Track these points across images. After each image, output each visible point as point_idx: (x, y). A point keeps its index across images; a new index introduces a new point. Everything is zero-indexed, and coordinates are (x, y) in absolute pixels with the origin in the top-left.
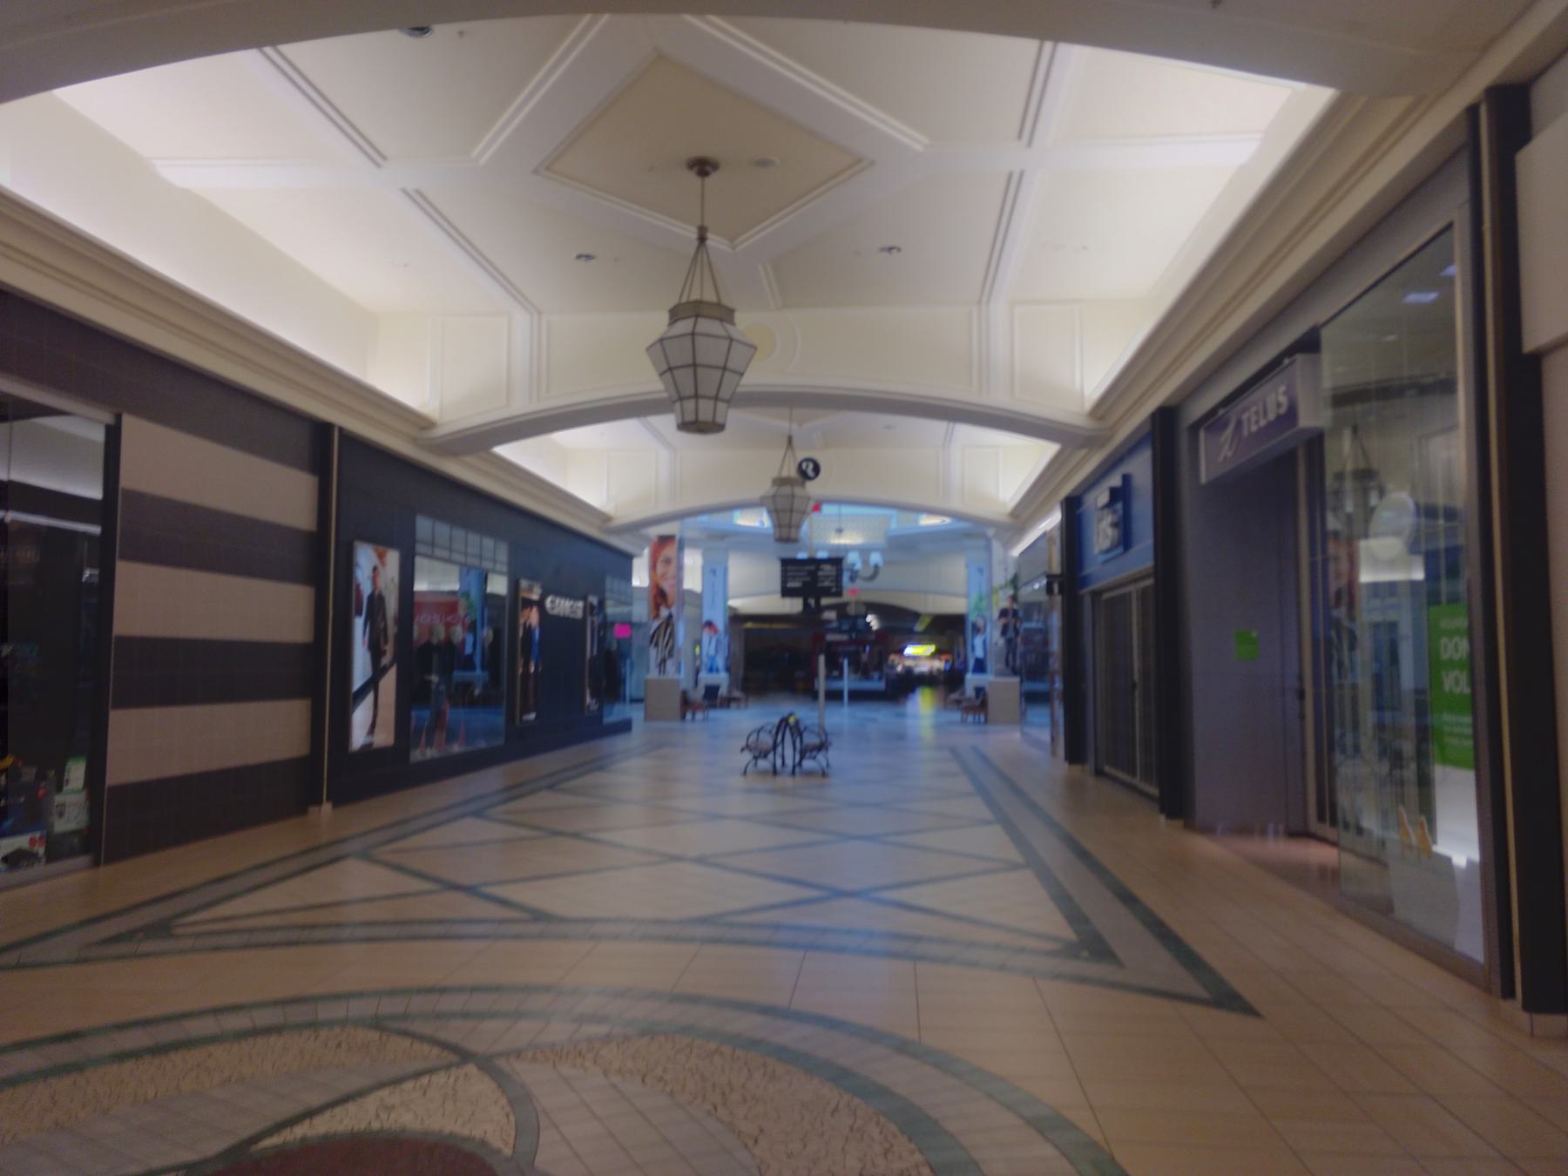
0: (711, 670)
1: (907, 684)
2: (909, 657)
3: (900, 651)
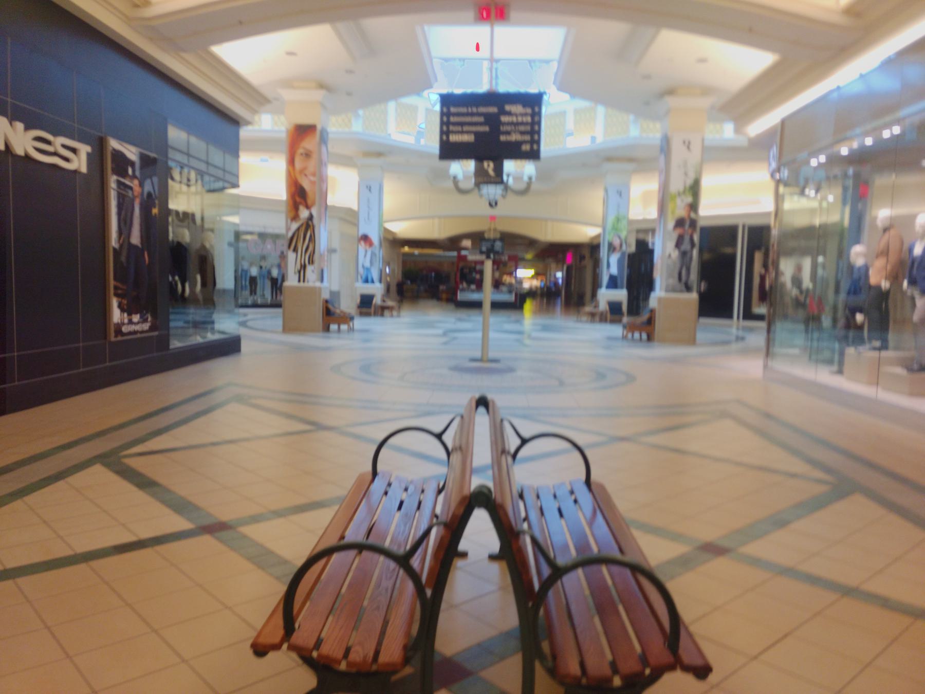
0: (366, 281)
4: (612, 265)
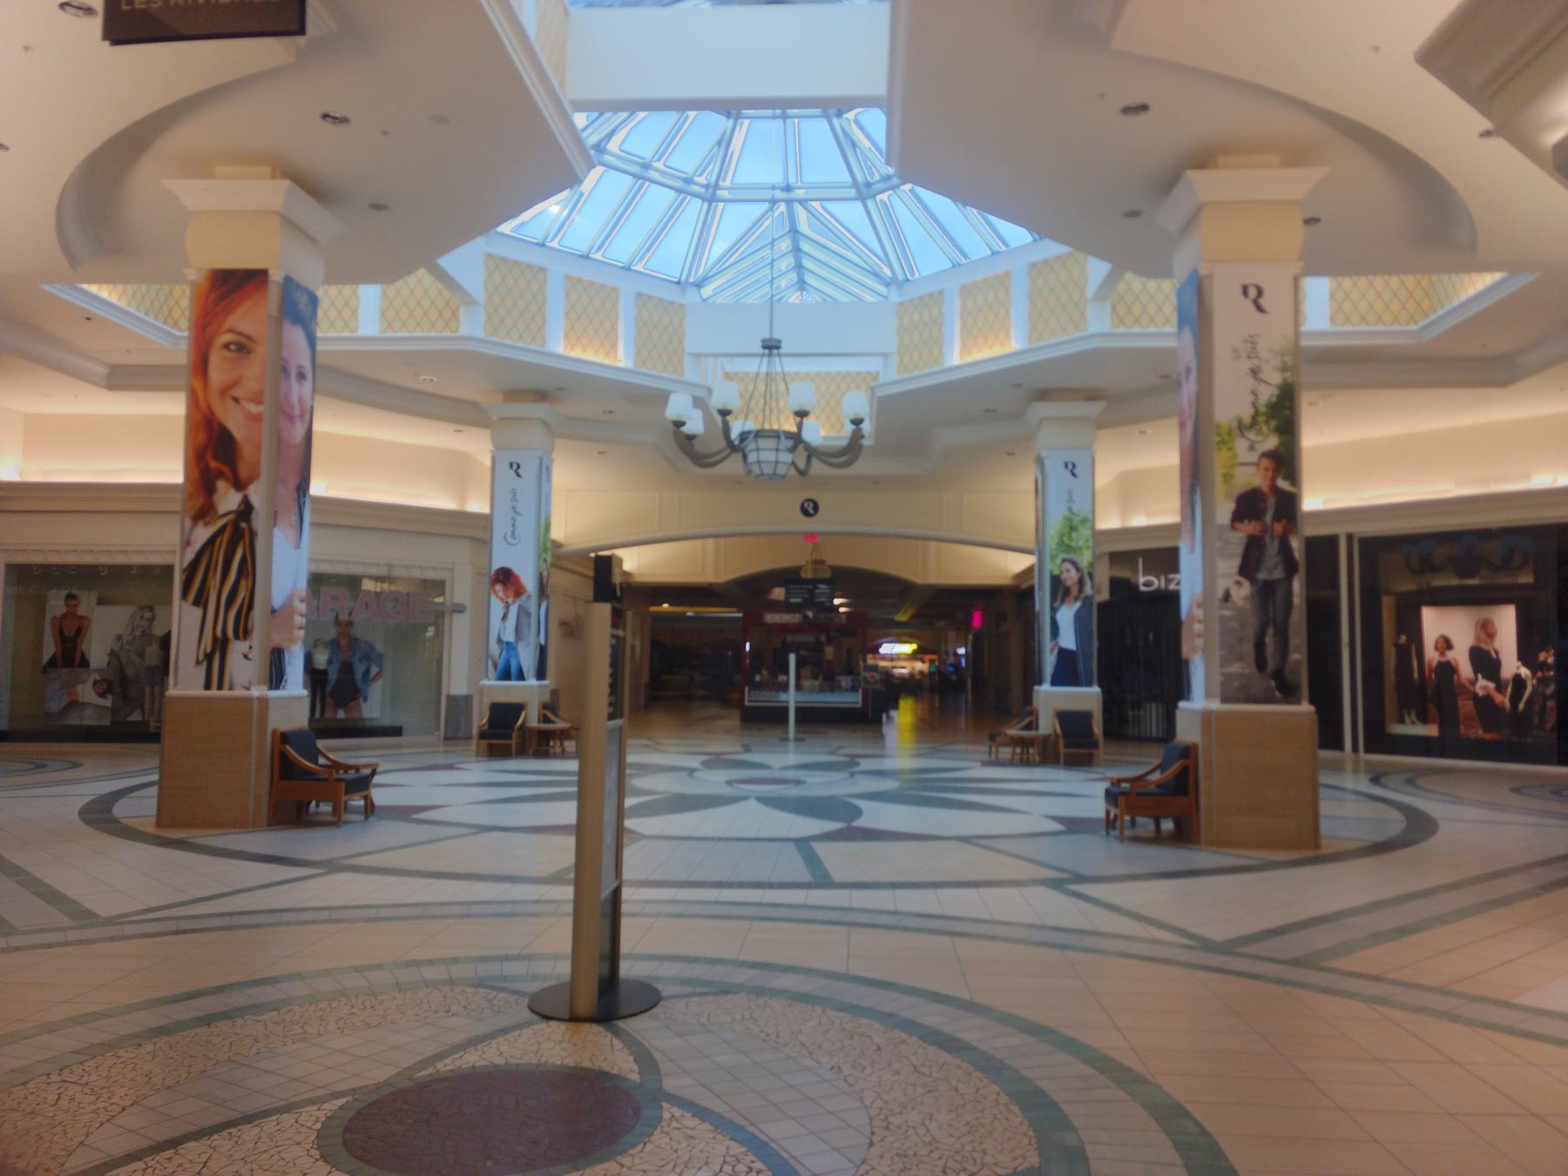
0: (506, 675)
1: (889, 691)
2: (884, 657)
3: (875, 650)
4: (1064, 628)
